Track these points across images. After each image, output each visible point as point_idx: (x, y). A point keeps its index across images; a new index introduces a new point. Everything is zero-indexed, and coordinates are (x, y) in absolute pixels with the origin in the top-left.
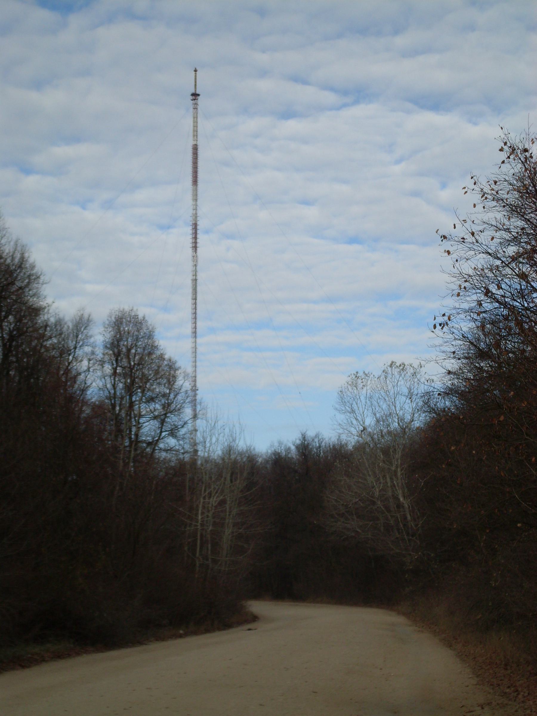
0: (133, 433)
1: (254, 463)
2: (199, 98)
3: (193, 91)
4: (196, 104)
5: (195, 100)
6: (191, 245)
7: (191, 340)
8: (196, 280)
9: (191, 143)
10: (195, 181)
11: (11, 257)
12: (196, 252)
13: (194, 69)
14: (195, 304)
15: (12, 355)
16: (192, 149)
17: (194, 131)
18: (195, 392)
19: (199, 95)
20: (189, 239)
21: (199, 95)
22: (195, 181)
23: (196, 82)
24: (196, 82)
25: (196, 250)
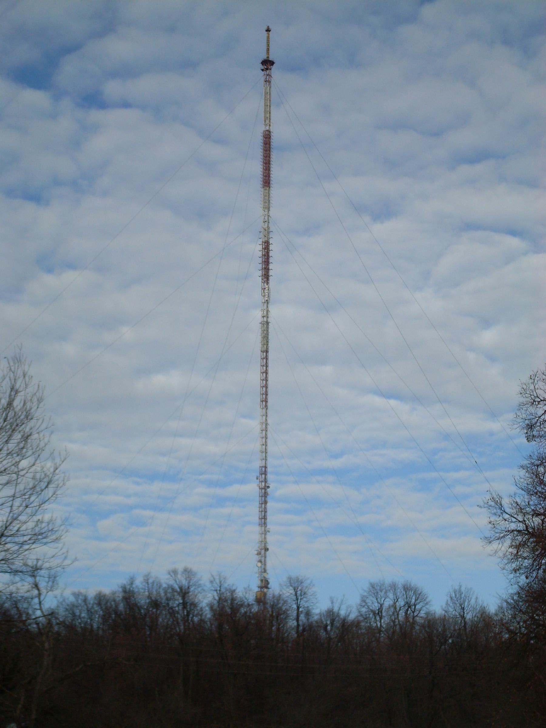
0: (179, 621)
1: (505, 604)
2: (274, 68)
3: (264, 56)
4: (269, 75)
5: (267, 69)
6: (260, 273)
7: (257, 529)
8: (268, 323)
9: (261, 129)
10: (266, 277)
11: (40, 406)
12: (268, 283)
13: (266, 28)
14: (267, 358)
15: (176, 630)
16: (262, 138)
17: (265, 112)
18: (265, 489)
19: (272, 63)
20: (258, 168)
21: (272, 63)
22: (266, 277)
23: (268, 45)
24: (268, 45)
25: (268, 279)
